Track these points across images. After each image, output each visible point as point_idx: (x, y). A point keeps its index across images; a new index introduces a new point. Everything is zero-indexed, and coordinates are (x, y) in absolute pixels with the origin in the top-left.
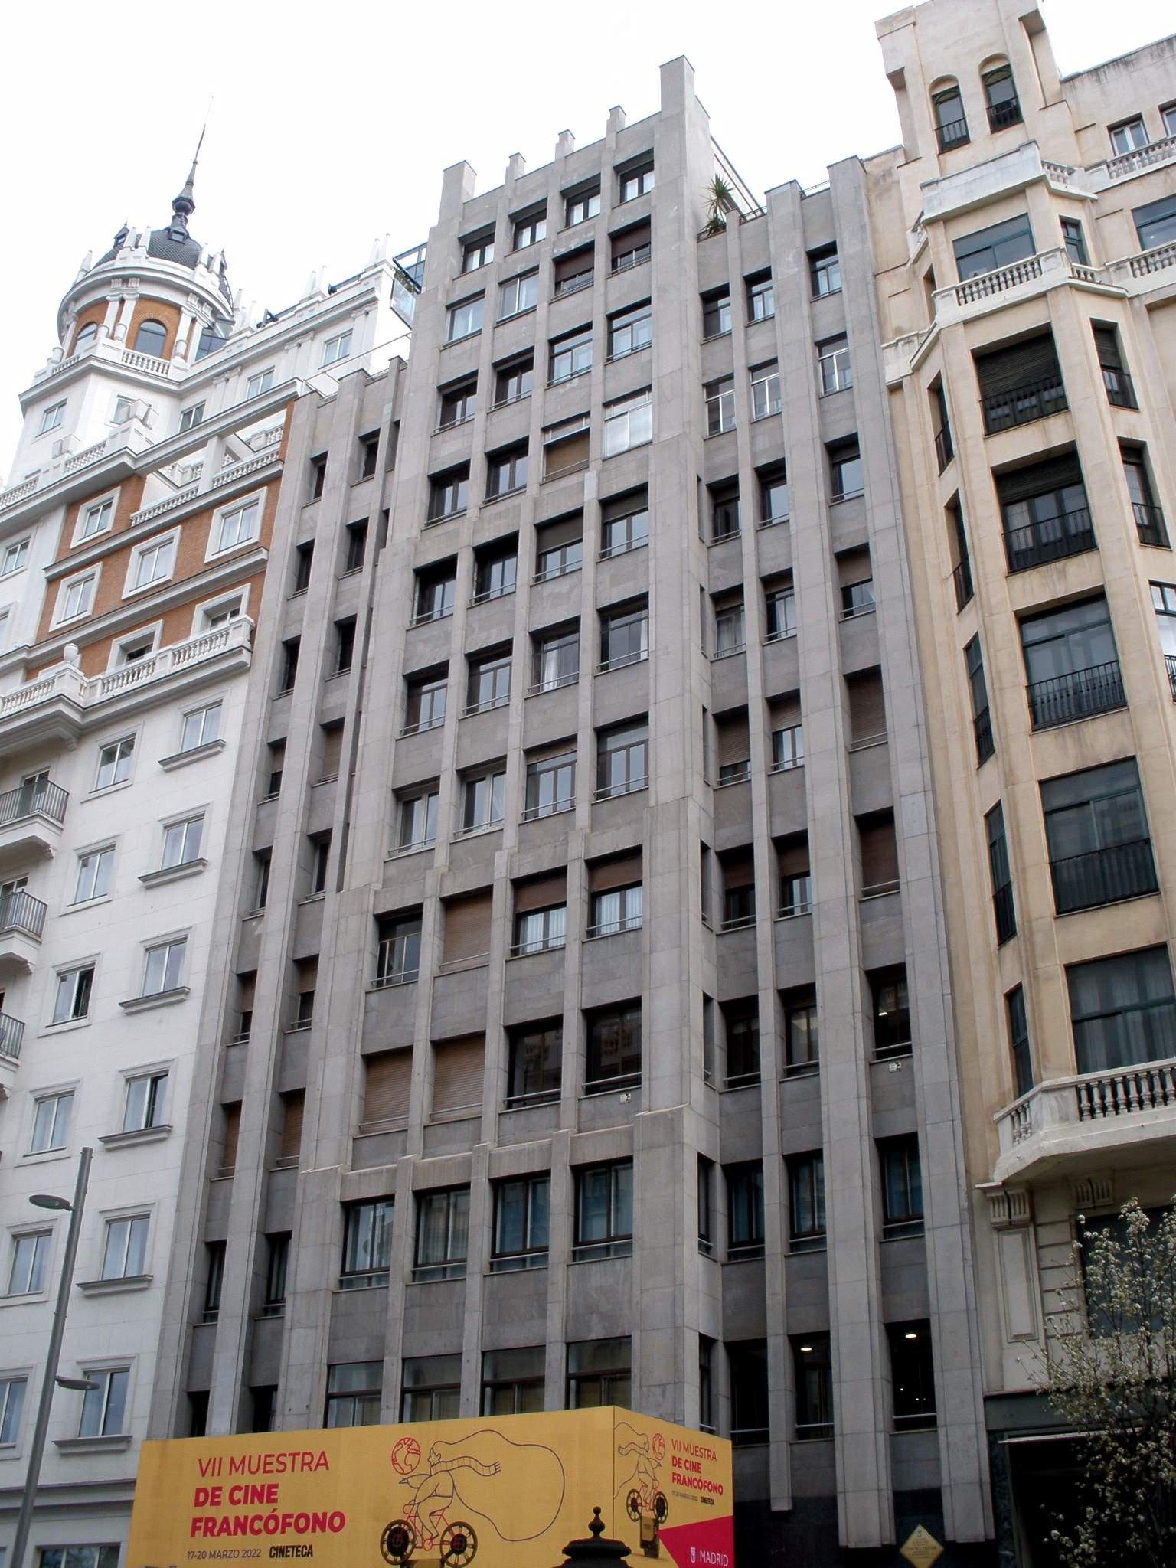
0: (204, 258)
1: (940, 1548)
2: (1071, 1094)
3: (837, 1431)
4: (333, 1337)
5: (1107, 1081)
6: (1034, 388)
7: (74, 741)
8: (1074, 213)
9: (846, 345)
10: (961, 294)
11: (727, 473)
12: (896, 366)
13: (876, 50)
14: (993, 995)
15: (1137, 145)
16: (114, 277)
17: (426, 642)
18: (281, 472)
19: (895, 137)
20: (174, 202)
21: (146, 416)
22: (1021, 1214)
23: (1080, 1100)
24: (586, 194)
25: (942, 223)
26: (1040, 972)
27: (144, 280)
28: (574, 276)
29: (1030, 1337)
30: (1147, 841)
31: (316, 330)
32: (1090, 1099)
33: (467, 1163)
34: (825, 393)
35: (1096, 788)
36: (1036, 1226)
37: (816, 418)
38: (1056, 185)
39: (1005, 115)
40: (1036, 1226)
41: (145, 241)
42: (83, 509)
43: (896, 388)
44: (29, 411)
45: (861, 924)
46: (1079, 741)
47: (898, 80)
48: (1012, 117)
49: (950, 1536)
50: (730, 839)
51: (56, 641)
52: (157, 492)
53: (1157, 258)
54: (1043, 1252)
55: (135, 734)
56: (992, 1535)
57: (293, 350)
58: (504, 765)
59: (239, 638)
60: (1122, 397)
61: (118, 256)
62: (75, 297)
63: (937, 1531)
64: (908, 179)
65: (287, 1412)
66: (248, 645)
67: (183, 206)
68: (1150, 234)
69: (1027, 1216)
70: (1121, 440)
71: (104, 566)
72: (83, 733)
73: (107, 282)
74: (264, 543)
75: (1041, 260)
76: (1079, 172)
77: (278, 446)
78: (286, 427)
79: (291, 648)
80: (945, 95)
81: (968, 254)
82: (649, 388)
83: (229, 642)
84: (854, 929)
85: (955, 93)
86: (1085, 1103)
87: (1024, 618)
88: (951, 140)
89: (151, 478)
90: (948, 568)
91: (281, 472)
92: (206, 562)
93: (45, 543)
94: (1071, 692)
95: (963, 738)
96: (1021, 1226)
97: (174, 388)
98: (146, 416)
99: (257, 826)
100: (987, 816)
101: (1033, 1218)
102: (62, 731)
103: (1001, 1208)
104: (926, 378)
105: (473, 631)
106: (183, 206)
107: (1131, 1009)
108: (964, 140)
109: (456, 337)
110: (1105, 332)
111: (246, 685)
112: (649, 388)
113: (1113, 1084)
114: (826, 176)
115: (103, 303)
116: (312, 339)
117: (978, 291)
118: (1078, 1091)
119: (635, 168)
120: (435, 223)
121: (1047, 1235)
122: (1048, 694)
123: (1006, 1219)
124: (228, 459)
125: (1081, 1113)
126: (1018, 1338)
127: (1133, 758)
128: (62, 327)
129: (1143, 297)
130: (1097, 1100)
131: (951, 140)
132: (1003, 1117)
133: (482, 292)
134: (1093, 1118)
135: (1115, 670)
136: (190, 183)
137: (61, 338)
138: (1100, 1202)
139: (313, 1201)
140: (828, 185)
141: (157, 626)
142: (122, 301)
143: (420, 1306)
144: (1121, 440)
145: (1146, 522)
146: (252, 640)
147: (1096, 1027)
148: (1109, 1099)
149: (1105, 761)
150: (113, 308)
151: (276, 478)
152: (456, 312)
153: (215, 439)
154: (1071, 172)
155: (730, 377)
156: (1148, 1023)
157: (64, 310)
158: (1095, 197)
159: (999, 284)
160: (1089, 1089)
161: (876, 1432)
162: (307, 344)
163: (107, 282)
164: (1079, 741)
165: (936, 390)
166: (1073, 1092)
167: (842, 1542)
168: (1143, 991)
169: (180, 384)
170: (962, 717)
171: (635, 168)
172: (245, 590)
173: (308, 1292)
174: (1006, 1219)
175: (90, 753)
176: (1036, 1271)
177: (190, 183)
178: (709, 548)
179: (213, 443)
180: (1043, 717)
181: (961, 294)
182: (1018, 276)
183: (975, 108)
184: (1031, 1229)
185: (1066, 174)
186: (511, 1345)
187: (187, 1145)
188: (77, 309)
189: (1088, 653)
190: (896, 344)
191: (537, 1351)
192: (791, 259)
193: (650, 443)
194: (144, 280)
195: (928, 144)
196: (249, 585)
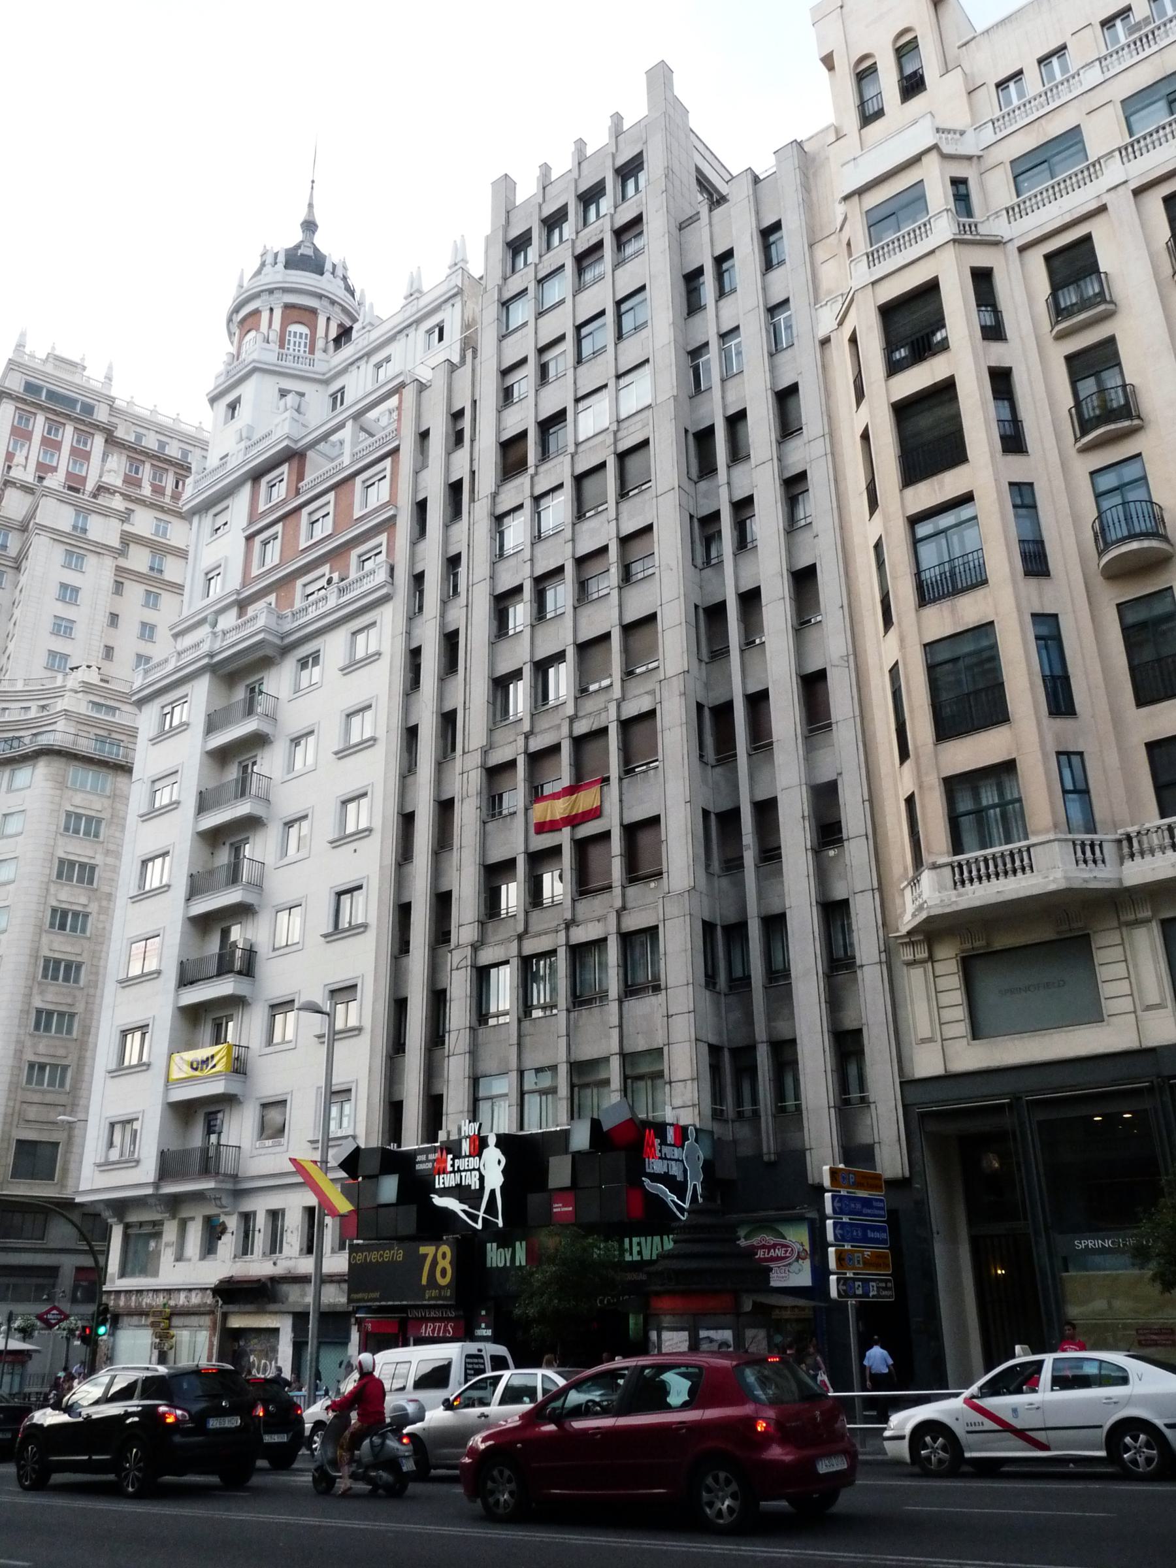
0: (328, 267)
2: (948, 870)
3: (804, 1107)
7: (278, 657)
8: (960, 171)
9: (789, 309)
10: (871, 258)
11: (707, 424)
12: (826, 321)
13: (811, 33)
14: (897, 800)
15: (1019, 98)
16: (262, 291)
18: (399, 445)
19: (828, 117)
20: (302, 224)
21: (299, 406)
22: (922, 954)
25: (857, 196)
26: (925, 784)
27: (285, 290)
29: (930, 1040)
32: (962, 873)
34: (776, 350)
35: (967, 647)
36: (933, 962)
37: (768, 374)
38: (947, 149)
39: (912, 86)
40: (933, 962)
41: (282, 259)
42: (264, 481)
43: (825, 342)
44: (215, 405)
45: (807, 753)
47: (828, 62)
48: (918, 86)
50: (716, 698)
52: (318, 470)
55: (319, 651)
56: (907, 1174)
58: (565, 655)
59: (382, 576)
60: (994, 332)
61: (263, 272)
62: (237, 310)
64: (837, 153)
66: (389, 580)
67: (310, 226)
68: (1024, 181)
69: (926, 955)
71: (284, 525)
72: (285, 650)
73: (256, 296)
74: (392, 502)
75: (932, 220)
76: (970, 133)
77: (395, 425)
78: (399, 408)
79: (418, 579)
80: (865, 73)
81: (878, 221)
82: (647, 361)
83: (376, 578)
84: (801, 757)
85: (873, 69)
86: (957, 876)
87: (914, 521)
88: (869, 116)
89: (310, 454)
90: (863, 485)
91: (399, 445)
92: (355, 518)
93: (239, 507)
94: (948, 574)
95: (875, 614)
96: (923, 962)
98: (299, 406)
99: (406, 709)
100: (890, 671)
102: (269, 652)
104: (847, 334)
106: (310, 226)
107: (994, 806)
108: (880, 113)
109: (511, 329)
110: (982, 278)
111: (391, 609)
112: (647, 361)
113: (986, 860)
114: (772, 160)
115: (256, 313)
117: (889, 252)
118: (953, 868)
119: (629, 170)
120: (489, 232)
121: (940, 968)
122: (936, 576)
123: (912, 957)
124: (363, 435)
125: (955, 883)
126: (924, 1041)
127: (992, 623)
128: (231, 334)
129: (1015, 241)
130: (966, 874)
131: (869, 116)
132: (907, 886)
133: (526, 289)
134: (963, 887)
135: (980, 555)
136: (311, 206)
137: (232, 343)
140: (774, 170)
142: (271, 310)
145: (1008, 433)
146: (392, 575)
148: (974, 873)
150: (265, 315)
151: (396, 450)
152: (511, 307)
153: (351, 421)
154: (962, 133)
155: (706, 344)
156: (1004, 816)
157: (230, 320)
158: (980, 153)
159: (900, 246)
160: (960, 866)
161: (829, 1108)
163: (256, 296)
164: (953, 611)
165: (853, 340)
166: (950, 868)
167: (810, 1182)
168: (1001, 794)
170: (873, 598)
171: (629, 170)
172: (383, 538)
174: (912, 957)
175: (289, 665)
176: (934, 994)
177: (311, 206)
178: (696, 483)
179: (349, 424)
180: (926, 595)
181: (871, 258)
182: (915, 236)
183: (888, 81)
184: (930, 964)
185: (958, 136)
187: (378, 934)
188: (239, 319)
189: (962, 542)
193: (649, 406)
194: (285, 290)
195: (852, 119)
196: (386, 534)
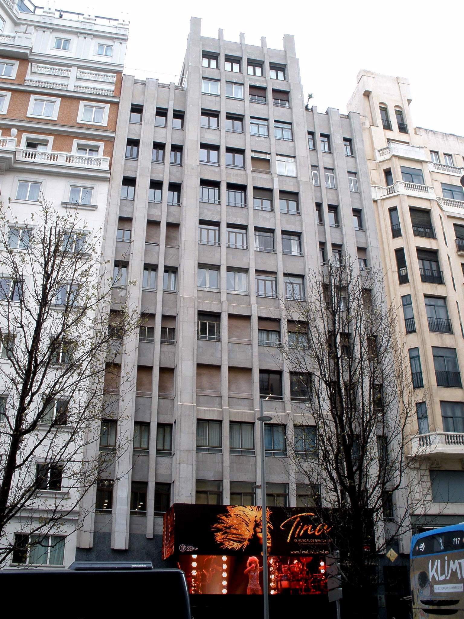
1: (397, 555)
4: (198, 469)
5: (452, 435)
6: (423, 227)
17: (208, 210)
23: (446, 439)
24: (256, 65)
28: (262, 97)
30: (459, 373)
31: (54, 30)
33: (221, 413)
46: (442, 339)
49: (401, 551)
51: (19, 122)
53: (449, 202)
54: (210, 445)
57: (81, 38)
63: (397, 550)
65: (180, 494)
70: (417, 247)
97: (16, 19)
101: (420, 467)
103: (214, 433)
105: (230, 215)
116: (51, 33)
138: (437, 466)
139: (186, 416)
141: (51, 139)
143: (236, 463)
144: (417, 247)
147: (450, 420)
149: (449, 347)
162: (47, 33)
169: (18, 19)
173: (187, 451)
186: (275, 482)
190: (375, 187)
191: (285, 486)
192: (339, 137)
